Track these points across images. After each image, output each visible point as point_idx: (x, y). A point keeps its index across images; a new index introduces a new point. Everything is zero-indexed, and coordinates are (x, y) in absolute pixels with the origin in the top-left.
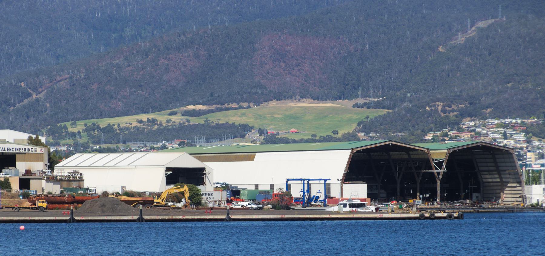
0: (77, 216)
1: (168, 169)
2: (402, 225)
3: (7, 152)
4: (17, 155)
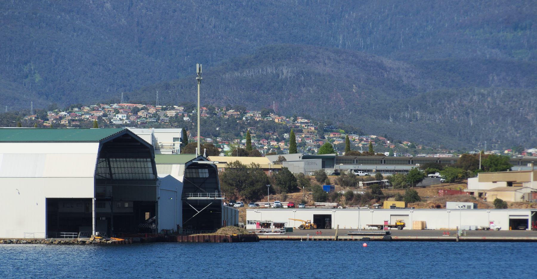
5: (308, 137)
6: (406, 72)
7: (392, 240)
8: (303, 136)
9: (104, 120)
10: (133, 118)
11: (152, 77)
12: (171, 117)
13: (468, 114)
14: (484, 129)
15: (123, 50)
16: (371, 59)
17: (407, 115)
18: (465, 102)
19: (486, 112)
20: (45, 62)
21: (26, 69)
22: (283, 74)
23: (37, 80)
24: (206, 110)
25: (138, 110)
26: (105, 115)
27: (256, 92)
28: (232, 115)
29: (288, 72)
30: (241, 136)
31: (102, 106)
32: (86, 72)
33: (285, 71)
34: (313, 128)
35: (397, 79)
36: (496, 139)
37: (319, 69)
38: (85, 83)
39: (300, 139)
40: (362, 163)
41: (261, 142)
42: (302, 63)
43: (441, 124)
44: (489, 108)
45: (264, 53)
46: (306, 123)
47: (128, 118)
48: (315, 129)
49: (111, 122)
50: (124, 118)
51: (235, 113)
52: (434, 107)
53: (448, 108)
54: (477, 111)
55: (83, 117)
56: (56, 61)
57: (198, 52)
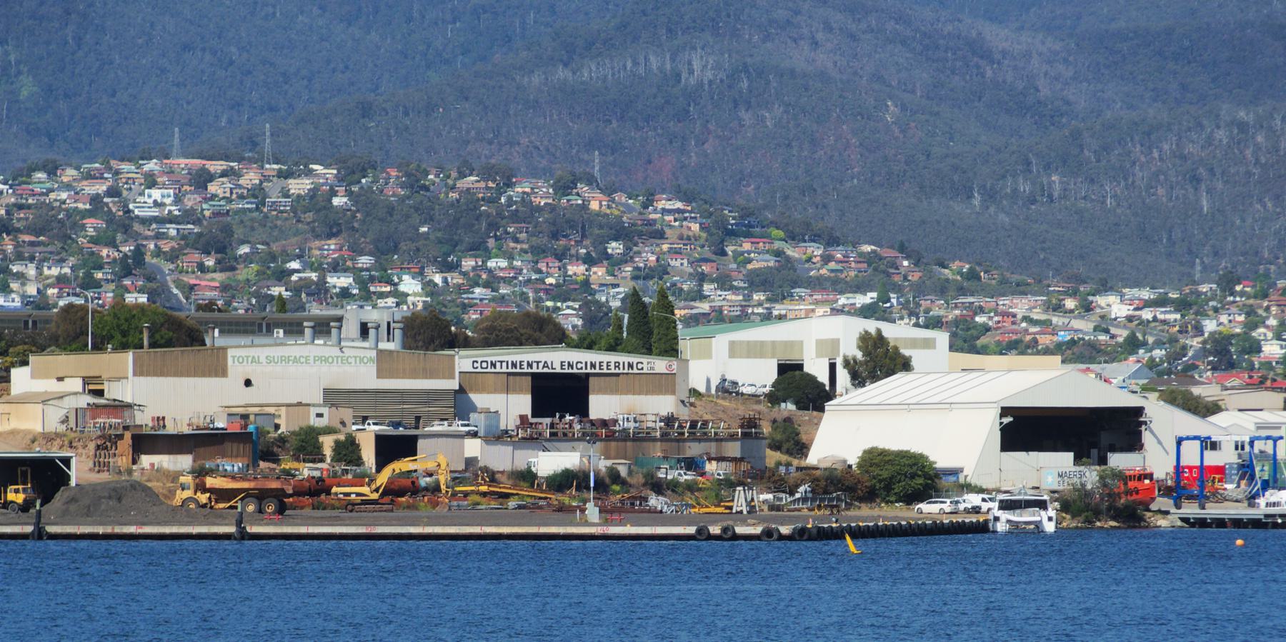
0: (252, 524)
1: (1005, 411)
2: (344, 554)
3: (558, 370)
4: (591, 379)
5: (678, 252)
6: (1049, 62)
7: (736, 537)
8: (665, 247)
9: (107, 204)
10: (191, 201)
11: (353, 84)
12: (299, 196)
13: (1196, 180)
14: (1238, 222)
15: (274, 6)
16: (950, 28)
17: (1025, 187)
18: (1190, 148)
19: (1249, 174)
20: (48, 43)
22: (691, 72)
23: (25, 93)
24: (398, 177)
25: (211, 178)
26: (113, 192)
27: (615, 124)
28: (468, 189)
29: (705, 67)
30: (487, 250)
31: (114, 163)
32: (164, 71)
33: (696, 65)
34: (695, 227)
35: (1020, 85)
36: (1271, 251)
37: (798, 57)
38: (158, 102)
39: (653, 258)
41: (542, 266)
42: (749, 41)
43: (1119, 211)
44: (1257, 162)
45: (644, 13)
46: (678, 211)
47: (178, 200)
48: (702, 228)
49: (129, 211)
50: (168, 201)
51: (482, 184)
52: (1104, 163)
53: (1141, 167)
54: (1223, 173)
55: (52, 196)
56: (79, 40)
57: (485, 12)
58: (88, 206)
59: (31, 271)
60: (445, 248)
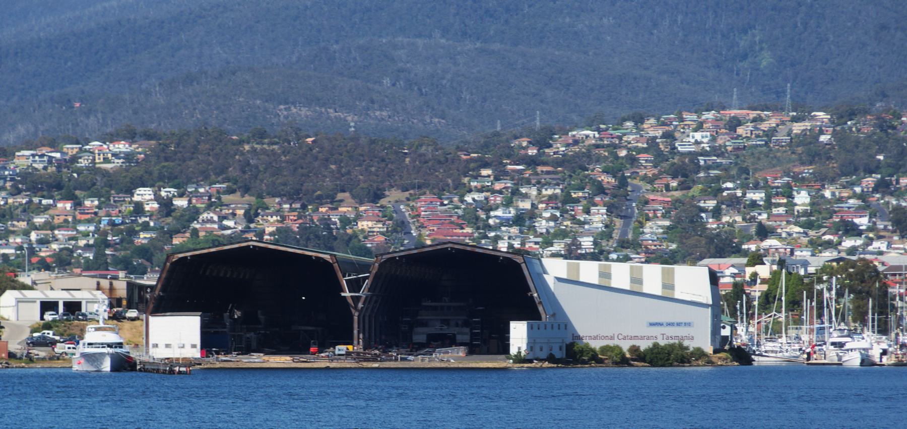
21: (743, 43)
23: (764, 63)
32: (864, 45)
40: (611, 347)
58: (645, 146)
59: (534, 192)
60: (890, 170)
